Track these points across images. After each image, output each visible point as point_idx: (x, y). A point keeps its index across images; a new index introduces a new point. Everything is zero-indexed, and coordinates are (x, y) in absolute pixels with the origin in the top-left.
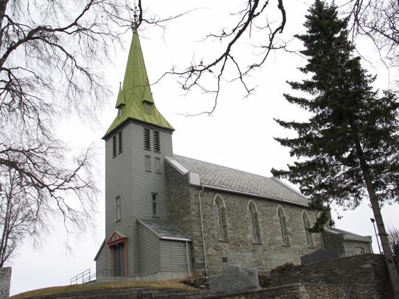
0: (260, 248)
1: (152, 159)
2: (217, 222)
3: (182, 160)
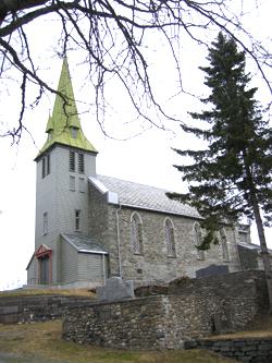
0: (174, 262)
1: (77, 180)
2: (134, 237)
3: (105, 181)
